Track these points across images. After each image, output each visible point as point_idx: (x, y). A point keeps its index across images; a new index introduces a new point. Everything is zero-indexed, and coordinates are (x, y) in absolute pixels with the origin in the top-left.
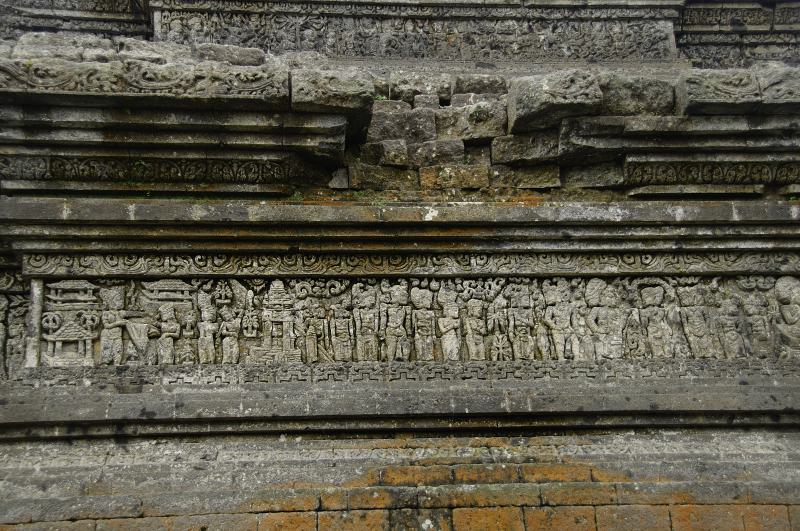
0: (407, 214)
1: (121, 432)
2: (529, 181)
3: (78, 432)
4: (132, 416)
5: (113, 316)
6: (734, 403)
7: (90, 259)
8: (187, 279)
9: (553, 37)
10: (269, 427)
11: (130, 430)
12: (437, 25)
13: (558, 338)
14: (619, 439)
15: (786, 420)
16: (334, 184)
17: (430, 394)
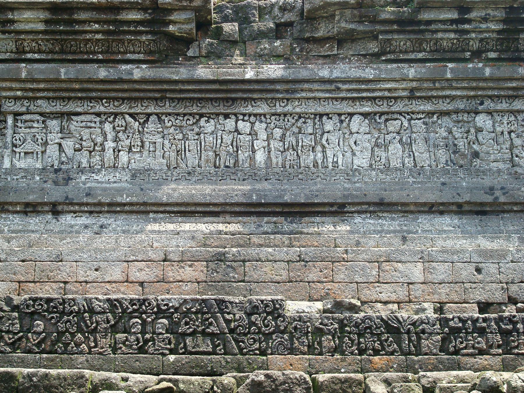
5: (54, 137)
7: (39, 102)
8: (98, 114)
15: (466, 208)
16: (190, 53)
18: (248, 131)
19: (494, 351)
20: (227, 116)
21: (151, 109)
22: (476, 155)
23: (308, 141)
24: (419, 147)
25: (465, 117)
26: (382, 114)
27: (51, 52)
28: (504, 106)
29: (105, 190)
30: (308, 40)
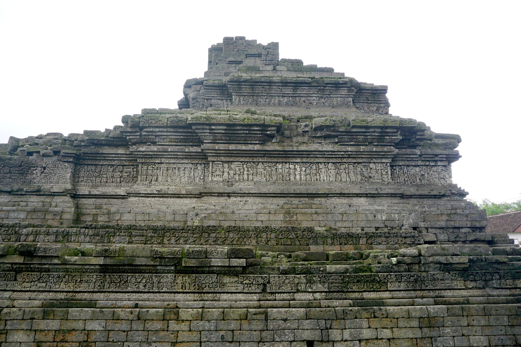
0: (290, 149)
1: (229, 195)
2: (316, 140)
3: (220, 195)
4: (231, 192)
5: (226, 170)
6: (358, 192)
7: (221, 157)
8: (241, 162)
9: (324, 101)
10: (259, 195)
11: (230, 195)
12: (297, 98)
13: (322, 176)
14: (333, 199)
15: (369, 195)
16: (273, 141)
17: (292, 189)
18: (293, 168)
19: (383, 243)
20: (286, 163)
21: (260, 160)
22: (370, 177)
23: (314, 172)
24: (352, 174)
25: (367, 164)
26: (339, 163)
27: (226, 140)
28: (379, 161)
29: (246, 188)
30: (314, 137)
